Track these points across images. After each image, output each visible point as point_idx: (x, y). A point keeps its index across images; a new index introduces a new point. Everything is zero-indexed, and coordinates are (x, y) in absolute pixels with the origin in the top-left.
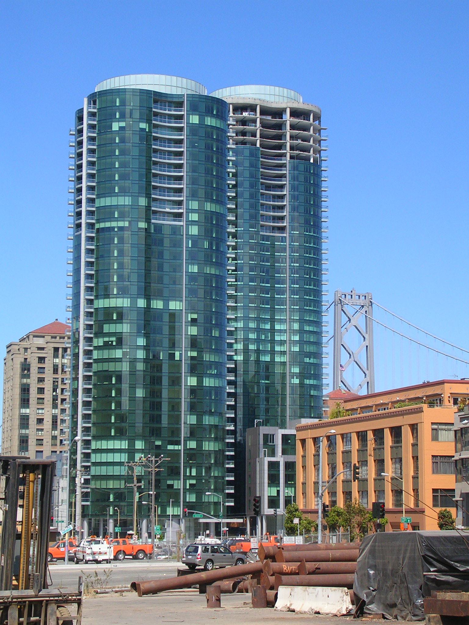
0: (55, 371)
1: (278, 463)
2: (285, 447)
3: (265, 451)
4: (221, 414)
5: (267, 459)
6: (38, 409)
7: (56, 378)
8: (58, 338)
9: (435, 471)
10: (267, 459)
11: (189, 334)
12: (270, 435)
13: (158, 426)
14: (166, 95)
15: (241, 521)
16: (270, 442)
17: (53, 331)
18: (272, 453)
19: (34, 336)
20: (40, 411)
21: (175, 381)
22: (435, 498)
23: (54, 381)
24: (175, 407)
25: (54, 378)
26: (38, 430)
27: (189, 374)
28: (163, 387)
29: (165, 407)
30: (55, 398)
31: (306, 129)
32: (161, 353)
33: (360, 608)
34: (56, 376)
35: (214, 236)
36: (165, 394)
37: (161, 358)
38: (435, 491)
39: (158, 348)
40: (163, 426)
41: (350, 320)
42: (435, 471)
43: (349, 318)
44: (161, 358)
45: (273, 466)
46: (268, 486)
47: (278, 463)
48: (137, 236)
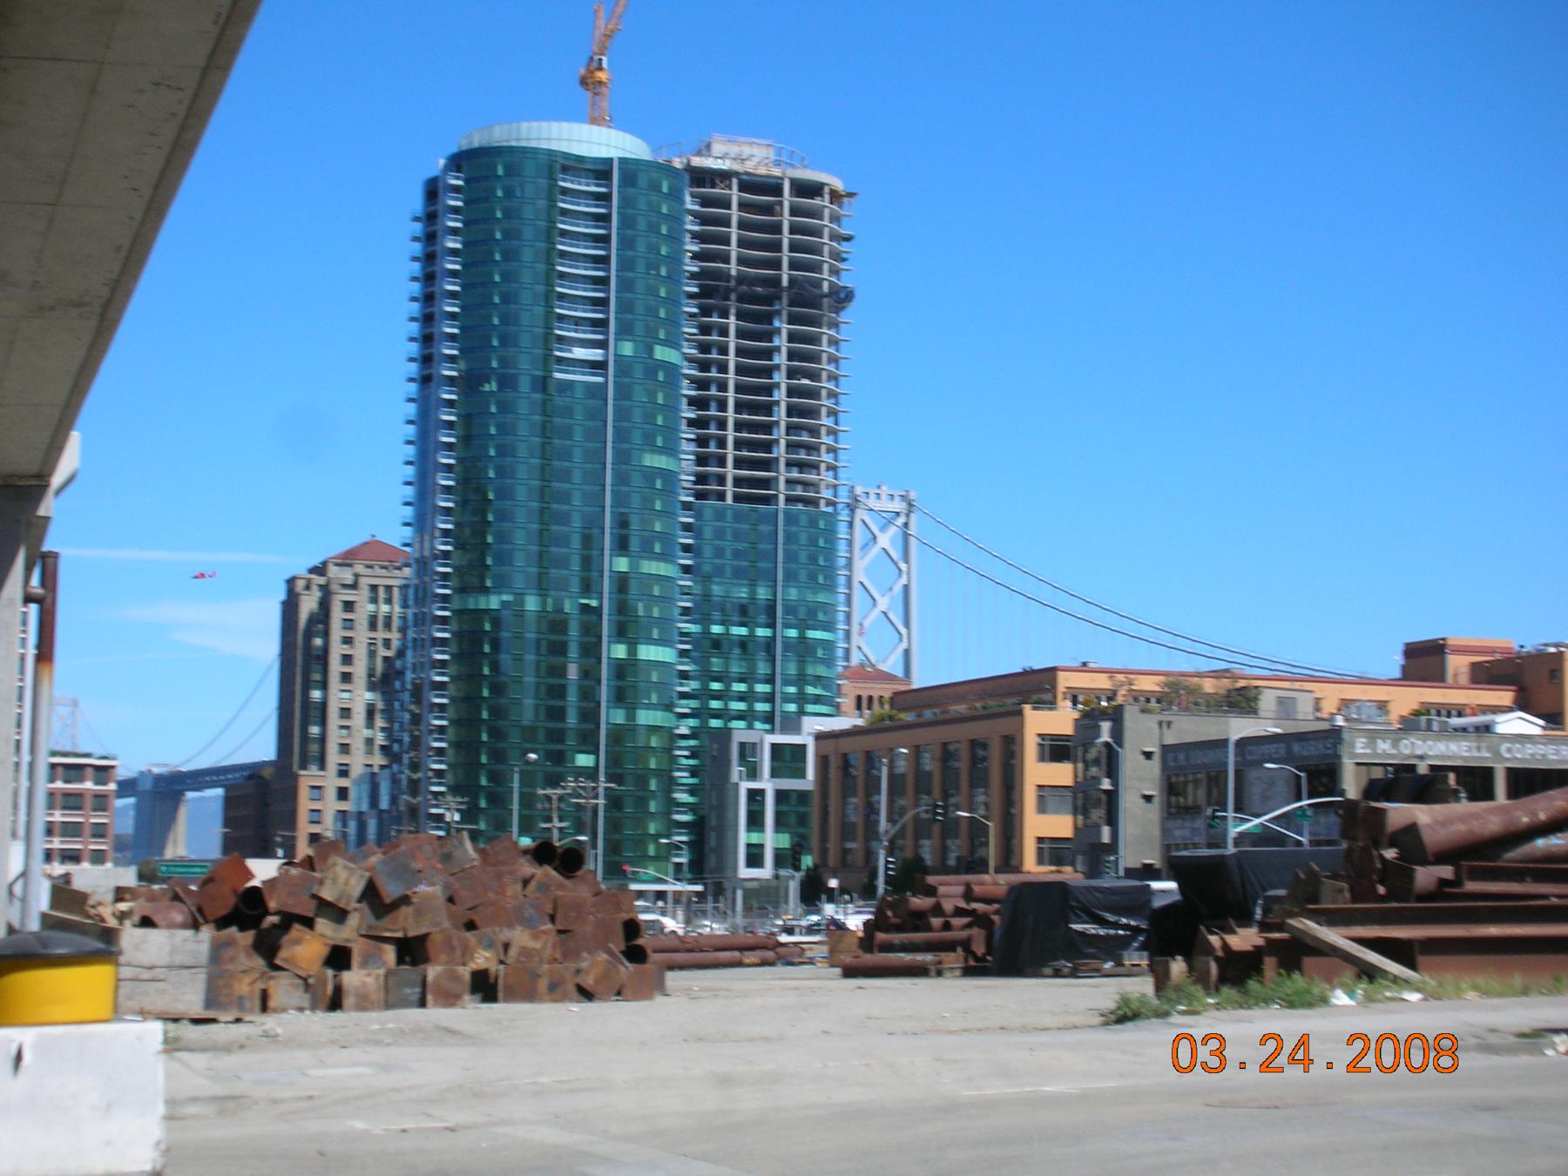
0: (373, 625)
1: (761, 792)
4: (668, 707)
5: (745, 786)
9: (1042, 808)
10: (745, 786)
13: (559, 725)
14: (580, 159)
15: (600, 379)
17: (369, 552)
18: (753, 773)
21: (591, 650)
22: (1040, 851)
24: (589, 694)
26: (342, 727)
29: (572, 697)
31: (814, 339)
33: (1425, 999)
34: (373, 635)
35: (660, 401)
38: (1040, 840)
42: (1042, 808)
45: (755, 796)
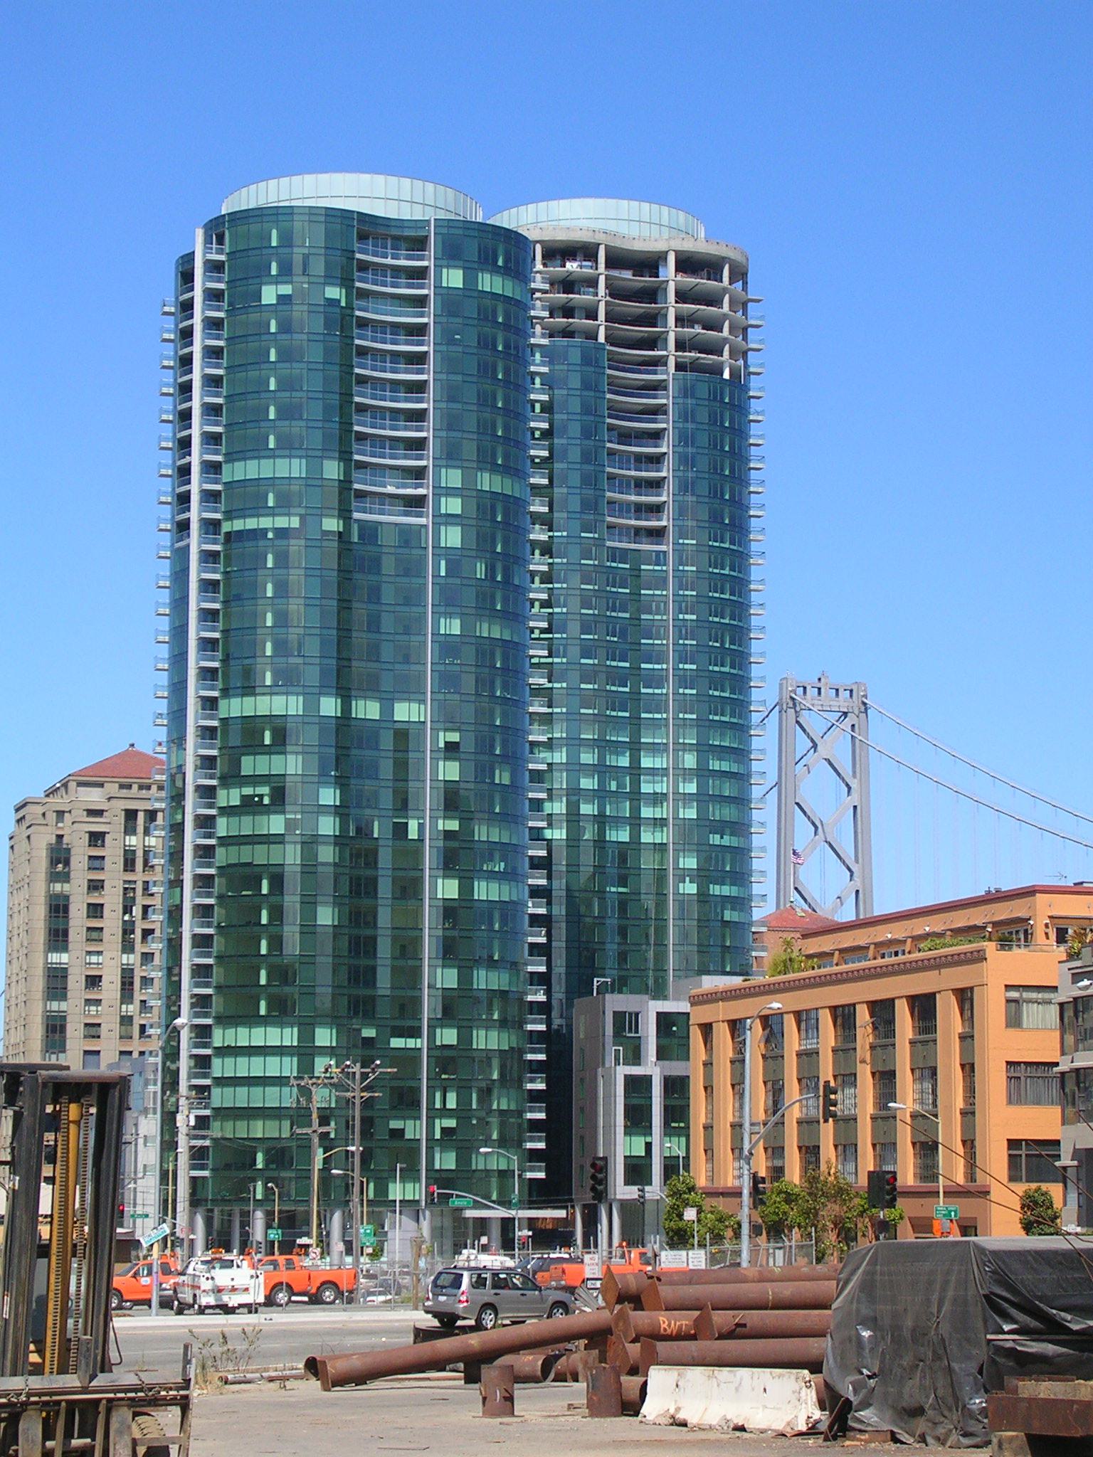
0: (129, 864)
1: (647, 1080)
2: (665, 1041)
3: (617, 1051)
4: (514, 966)
5: (623, 1071)
6: (89, 953)
7: (130, 882)
8: (135, 787)
9: (1015, 1098)
10: (623, 1071)
11: (441, 778)
12: (630, 1014)
13: (368, 992)
14: (386, 222)
15: (561, 1214)
16: (630, 1031)
17: (123, 771)
18: (635, 1056)
19: (80, 784)
20: (94, 959)
21: (409, 889)
22: (1013, 1161)
23: (125, 889)
24: (407, 948)
25: (125, 882)
26: (88, 1002)
27: (441, 873)
28: (380, 902)
29: (385, 949)
30: (129, 928)
31: (712, 300)
32: (376, 824)
34: (130, 877)
35: (499, 550)
36: (384, 918)
37: (376, 835)
38: (1013, 1144)
39: (368, 812)
40: (380, 992)
41: (815, 746)
42: (1015, 1098)
43: (812, 741)
44: (376, 835)
45: (637, 1086)
46: (625, 1134)
47: (647, 1080)
48: (318, 550)
